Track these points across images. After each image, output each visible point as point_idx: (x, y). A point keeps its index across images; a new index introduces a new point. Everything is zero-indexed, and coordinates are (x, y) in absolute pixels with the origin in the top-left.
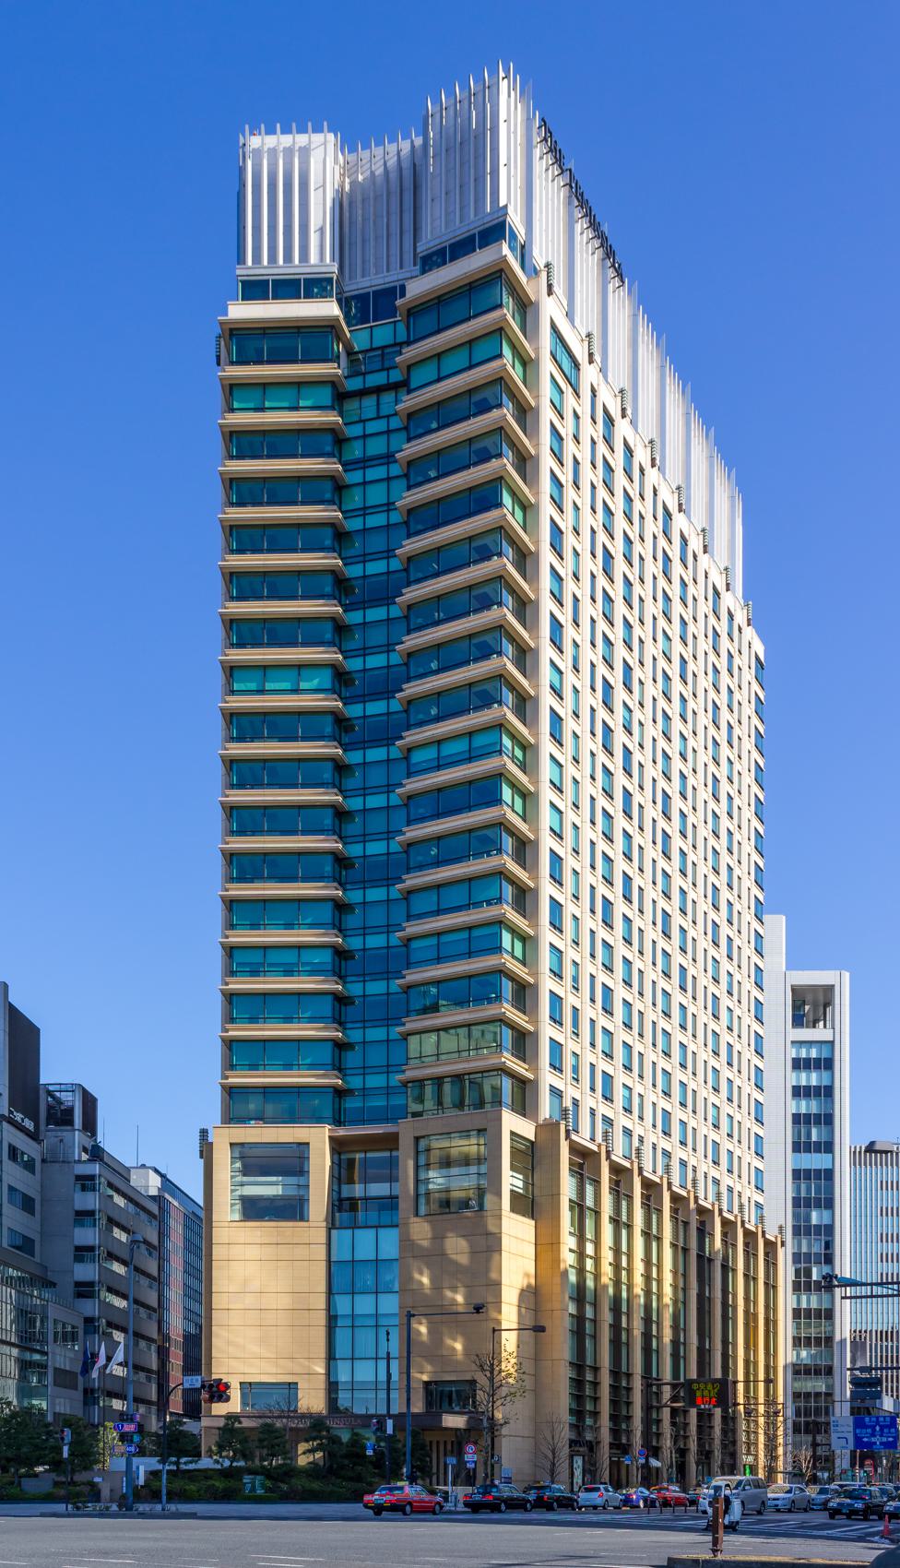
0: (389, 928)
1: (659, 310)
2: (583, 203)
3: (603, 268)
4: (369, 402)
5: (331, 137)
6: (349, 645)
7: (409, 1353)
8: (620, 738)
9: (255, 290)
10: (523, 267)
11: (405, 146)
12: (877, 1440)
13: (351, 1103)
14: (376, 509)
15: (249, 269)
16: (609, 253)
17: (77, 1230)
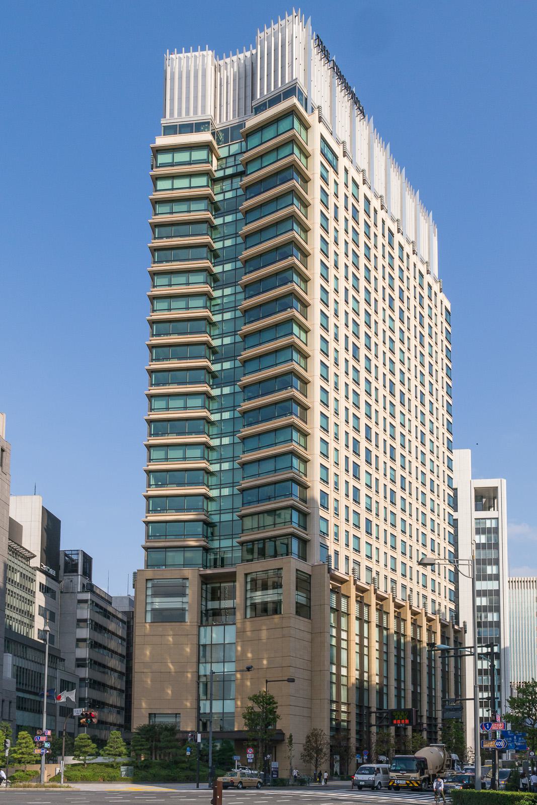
1: (386, 132)
2: (341, 77)
3: (352, 109)
4: (228, 182)
5: (210, 53)
8: (398, 387)
9: (171, 130)
10: (306, 110)
11: (248, 54)
15: (166, 121)
16: (355, 100)
17: (78, 630)
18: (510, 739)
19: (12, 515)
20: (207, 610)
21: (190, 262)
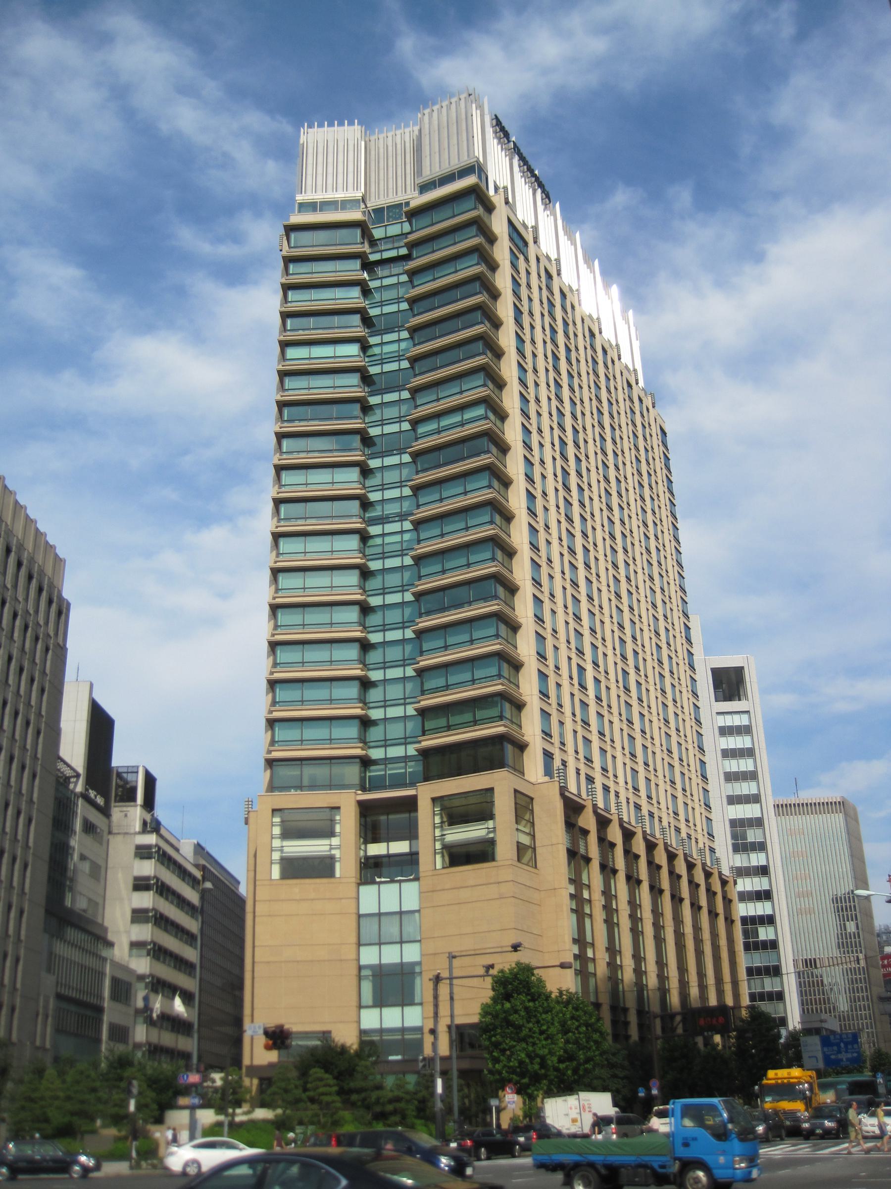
6: (369, 483)
7: (298, 962)
13: (375, 772)
16: (538, 183)
18: (835, 1048)
21: (439, 371)
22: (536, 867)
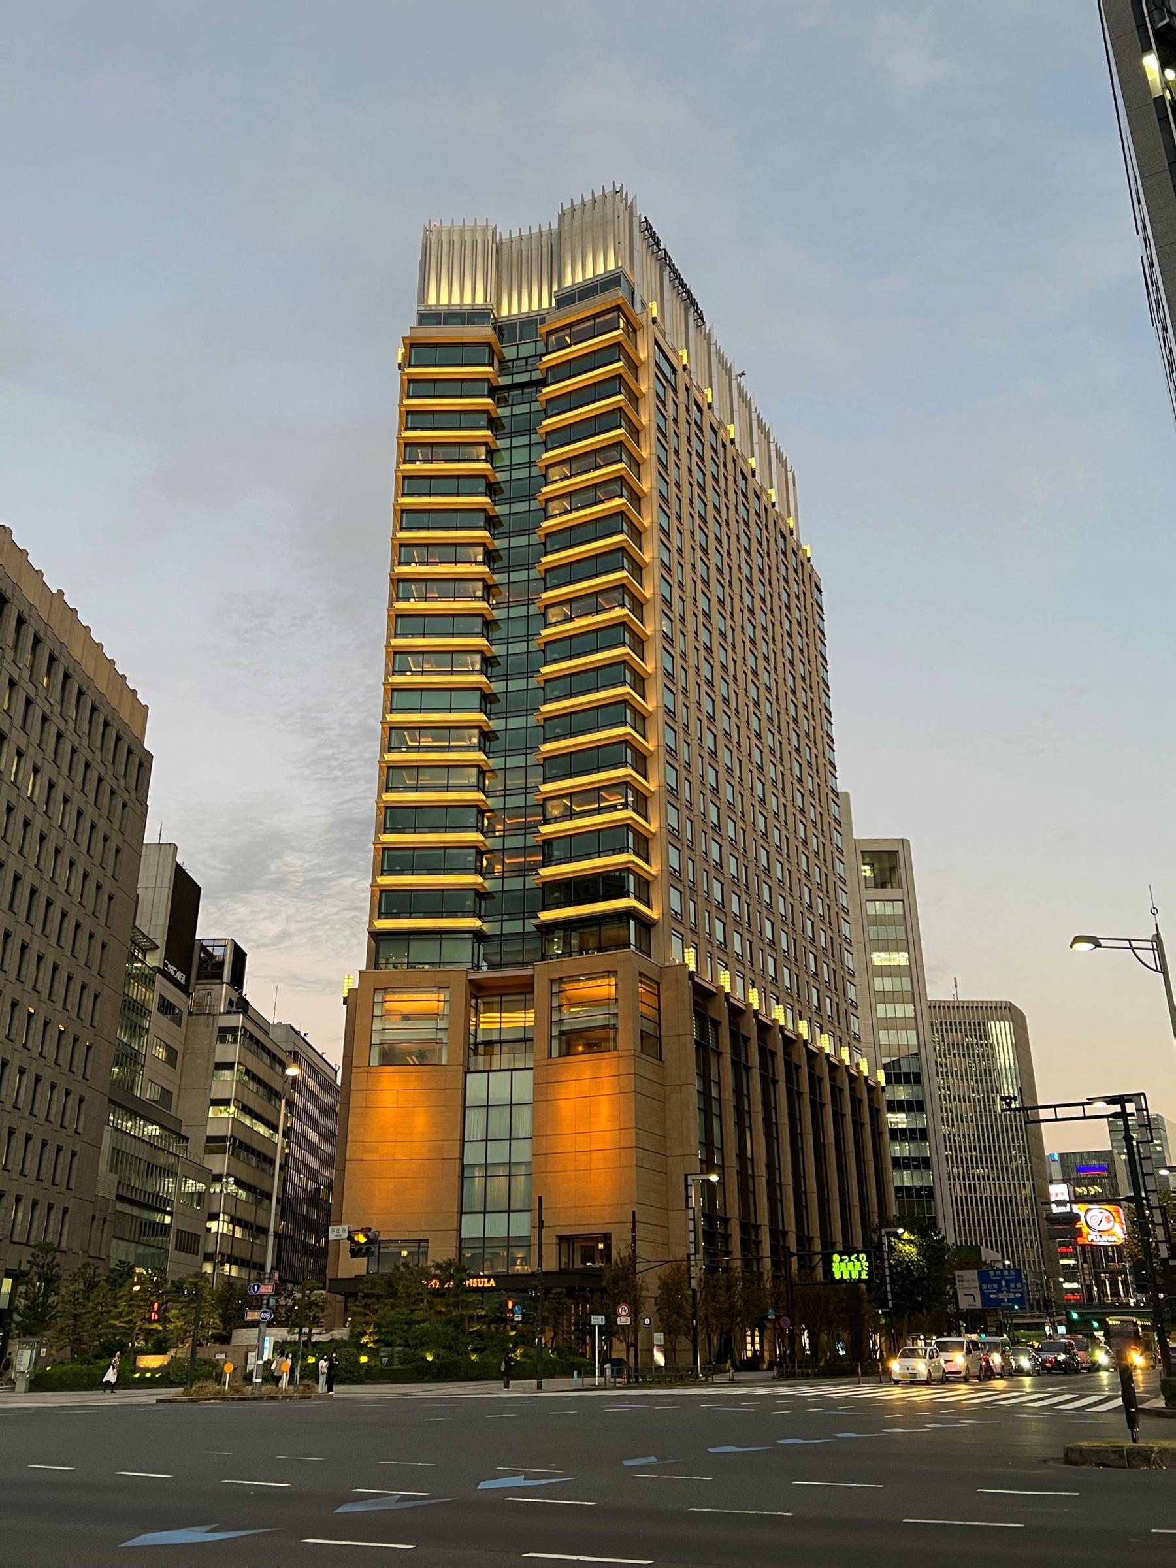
0: (528, 638)
6: (494, 635)
12: (1003, 1296)
14: (520, 466)
18: (995, 1286)
19: (179, 860)
20: (476, 1044)
22: (661, 1059)
